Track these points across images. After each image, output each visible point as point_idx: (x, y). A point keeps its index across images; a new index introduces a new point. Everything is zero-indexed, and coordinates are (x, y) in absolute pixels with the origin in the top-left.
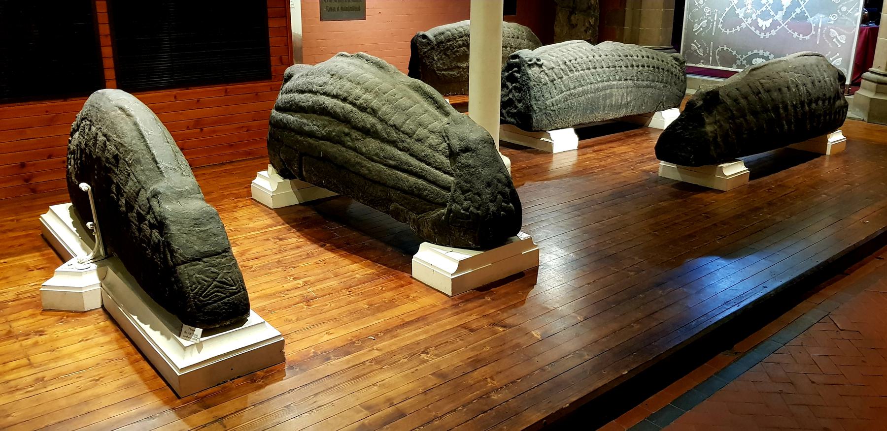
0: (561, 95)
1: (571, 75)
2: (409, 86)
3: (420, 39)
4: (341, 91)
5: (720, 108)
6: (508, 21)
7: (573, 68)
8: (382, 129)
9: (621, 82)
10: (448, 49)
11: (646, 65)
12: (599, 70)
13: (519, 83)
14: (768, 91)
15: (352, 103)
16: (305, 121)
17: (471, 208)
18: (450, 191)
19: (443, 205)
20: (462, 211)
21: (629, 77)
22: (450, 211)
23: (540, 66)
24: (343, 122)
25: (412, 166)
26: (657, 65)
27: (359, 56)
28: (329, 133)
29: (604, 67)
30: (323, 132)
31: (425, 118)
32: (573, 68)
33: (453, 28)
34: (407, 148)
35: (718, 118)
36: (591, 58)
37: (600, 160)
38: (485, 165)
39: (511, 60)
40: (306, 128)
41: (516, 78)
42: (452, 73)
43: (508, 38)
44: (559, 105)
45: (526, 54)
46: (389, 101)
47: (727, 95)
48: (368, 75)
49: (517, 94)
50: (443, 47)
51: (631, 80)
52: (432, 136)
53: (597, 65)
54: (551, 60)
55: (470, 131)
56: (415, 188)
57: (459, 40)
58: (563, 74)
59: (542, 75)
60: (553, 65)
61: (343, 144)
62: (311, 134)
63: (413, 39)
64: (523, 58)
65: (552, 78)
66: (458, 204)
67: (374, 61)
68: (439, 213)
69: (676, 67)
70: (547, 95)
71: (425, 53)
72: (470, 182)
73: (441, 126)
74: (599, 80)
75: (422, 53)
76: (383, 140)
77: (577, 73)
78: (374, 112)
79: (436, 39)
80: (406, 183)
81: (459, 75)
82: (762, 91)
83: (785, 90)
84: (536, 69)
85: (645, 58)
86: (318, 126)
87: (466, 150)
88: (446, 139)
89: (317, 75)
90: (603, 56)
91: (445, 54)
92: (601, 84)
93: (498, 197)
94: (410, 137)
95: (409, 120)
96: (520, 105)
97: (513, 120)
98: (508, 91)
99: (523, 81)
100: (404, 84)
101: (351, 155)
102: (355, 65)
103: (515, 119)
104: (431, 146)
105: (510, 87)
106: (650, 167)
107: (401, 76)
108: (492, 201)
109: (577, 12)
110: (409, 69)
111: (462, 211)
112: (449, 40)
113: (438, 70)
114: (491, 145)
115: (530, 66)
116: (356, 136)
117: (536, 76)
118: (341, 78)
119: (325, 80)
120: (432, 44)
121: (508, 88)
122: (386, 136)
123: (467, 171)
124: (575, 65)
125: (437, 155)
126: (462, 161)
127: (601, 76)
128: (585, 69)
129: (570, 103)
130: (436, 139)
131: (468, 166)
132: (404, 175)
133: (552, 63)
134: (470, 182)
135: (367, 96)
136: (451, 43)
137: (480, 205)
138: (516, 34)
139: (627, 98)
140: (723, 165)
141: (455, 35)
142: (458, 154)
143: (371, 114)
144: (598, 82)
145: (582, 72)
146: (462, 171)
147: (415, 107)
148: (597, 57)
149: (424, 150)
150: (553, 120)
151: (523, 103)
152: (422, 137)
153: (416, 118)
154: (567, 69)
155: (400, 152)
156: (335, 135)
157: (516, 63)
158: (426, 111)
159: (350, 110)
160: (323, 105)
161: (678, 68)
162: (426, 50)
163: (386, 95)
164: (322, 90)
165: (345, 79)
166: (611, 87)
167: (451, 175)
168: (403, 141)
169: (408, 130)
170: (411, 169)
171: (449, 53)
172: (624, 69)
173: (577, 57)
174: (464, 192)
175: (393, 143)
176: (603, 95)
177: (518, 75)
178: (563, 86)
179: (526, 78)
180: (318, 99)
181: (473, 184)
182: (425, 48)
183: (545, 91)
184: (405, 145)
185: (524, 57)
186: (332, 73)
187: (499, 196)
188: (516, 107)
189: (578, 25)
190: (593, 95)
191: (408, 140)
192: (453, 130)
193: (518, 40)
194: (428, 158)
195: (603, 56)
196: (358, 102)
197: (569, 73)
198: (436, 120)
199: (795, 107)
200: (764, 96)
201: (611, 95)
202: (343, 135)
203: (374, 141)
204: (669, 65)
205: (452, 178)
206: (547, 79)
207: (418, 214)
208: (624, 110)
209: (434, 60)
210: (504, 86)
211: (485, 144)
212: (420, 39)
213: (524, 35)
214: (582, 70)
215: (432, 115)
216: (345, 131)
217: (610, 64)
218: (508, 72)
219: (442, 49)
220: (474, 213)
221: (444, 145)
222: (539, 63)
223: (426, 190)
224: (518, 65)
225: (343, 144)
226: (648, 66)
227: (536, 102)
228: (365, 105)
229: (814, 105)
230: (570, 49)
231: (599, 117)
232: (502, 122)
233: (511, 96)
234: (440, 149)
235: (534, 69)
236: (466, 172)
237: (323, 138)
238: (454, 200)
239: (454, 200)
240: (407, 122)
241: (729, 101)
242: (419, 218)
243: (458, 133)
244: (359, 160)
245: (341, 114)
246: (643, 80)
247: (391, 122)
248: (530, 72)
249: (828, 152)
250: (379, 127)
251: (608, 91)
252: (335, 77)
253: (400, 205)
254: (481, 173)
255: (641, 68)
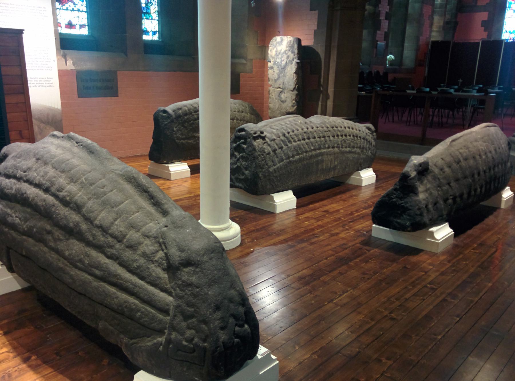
0: (281, 163)
1: (290, 145)
2: (121, 176)
3: (161, 113)
4: (44, 179)
5: (429, 177)
6: (234, 99)
7: (291, 139)
8: (87, 230)
9: (329, 150)
10: (185, 121)
11: (348, 134)
12: (312, 140)
13: (246, 153)
14: (466, 159)
15: (54, 195)
16: (9, 211)
17: (196, 340)
18: (168, 315)
19: (160, 332)
20: (184, 343)
21: (336, 145)
22: (169, 341)
23: (264, 138)
24: (45, 217)
25: (122, 279)
26: (356, 134)
27: (70, 138)
28: (31, 228)
29: (316, 137)
30: (24, 226)
31: (137, 217)
32: (291, 139)
33: (189, 104)
34: (115, 255)
35: (429, 186)
36: (305, 130)
37: (318, 219)
38: (213, 282)
39: (238, 133)
40: (9, 219)
41: (243, 149)
42: (190, 141)
43: (235, 113)
44: (280, 172)
45: (251, 127)
46: (97, 196)
47: (435, 165)
48: (75, 161)
49: (244, 163)
50: (181, 120)
51: (337, 147)
52: (147, 241)
53: (311, 136)
54: (273, 133)
55: (194, 238)
56: (125, 307)
57: (194, 114)
58: (283, 145)
59: (265, 146)
60: (274, 137)
61: (44, 242)
62: (13, 227)
63: (155, 114)
64: (248, 131)
65: (274, 148)
66: (178, 333)
67: (84, 144)
68: (155, 341)
69: (369, 135)
70: (270, 163)
71: (166, 125)
72: (192, 305)
73: (157, 230)
74: (312, 148)
75: (163, 125)
76: (88, 244)
77: (294, 144)
78: (78, 208)
79: (175, 113)
80: (115, 300)
81: (195, 143)
82: (462, 159)
83: (478, 157)
84: (260, 141)
85: (347, 129)
86: (20, 219)
87: (187, 263)
88: (164, 247)
89: (23, 158)
90: (315, 128)
91: (183, 126)
92: (314, 153)
93: (230, 321)
94: (119, 242)
95: (118, 220)
96: (247, 172)
97: (241, 185)
98: (236, 160)
99: (250, 151)
100: (116, 173)
101: (52, 257)
102: (63, 148)
103: (243, 184)
104: (144, 255)
105: (238, 157)
106: (361, 225)
107: (113, 163)
108: (222, 328)
109: (286, 92)
110: (153, 138)
111: (184, 343)
112: (186, 114)
113: (177, 139)
114: (220, 255)
115: (255, 138)
116: (58, 236)
117: (260, 146)
118: (46, 163)
119: (30, 165)
120: (172, 118)
121: (236, 157)
122: (91, 239)
123: (189, 290)
124: (293, 136)
125: (152, 266)
126: (183, 278)
127: (314, 145)
128: (301, 139)
129: (289, 170)
130: (151, 246)
131: (191, 285)
132: (112, 290)
133: (273, 135)
134: (192, 305)
135: (72, 188)
136: (188, 116)
137: (207, 336)
138: (241, 109)
139: (334, 163)
140: (432, 229)
141: (191, 110)
142: (178, 269)
143: (75, 210)
144: (312, 150)
145: (298, 142)
146: (184, 291)
147: (127, 204)
148: (310, 129)
149: (136, 260)
150: (275, 184)
151: (249, 171)
152: (134, 243)
153: (127, 218)
154: (286, 140)
155: (107, 261)
156: (37, 232)
157: (243, 135)
158: (140, 208)
159: (52, 203)
160: (25, 195)
161: (371, 135)
162: (166, 123)
163: (94, 186)
164: (26, 176)
165: (50, 166)
166: (322, 154)
167: (170, 294)
168: (111, 247)
169: (117, 233)
170: (120, 283)
171: (186, 125)
172: (332, 138)
173: (294, 129)
174: (186, 317)
175: (100, 248)
176: (316, 161)
177: (245, 146)
178: (283, 155)
179: (251, 149)
180: (21, 186)
181: (198, 308)
182: (166, 121)
183: (268, 160)
184: (114, 251)
185: (249, 130)
186: (38, 157)
187: (231, 320)
188: (243, 174)
189: (287, 101)
190: (307, 161)
191: (118, 246)
192: (172, 235)
193: (243, 114)
194: (141, 271)
195: (315, 128)
196: (61, 194)
197: (288, 144)
198: (152, 220)
199: (485, 172)
200: (463, 163)
201: (322, 161)
202: (45, 232)
203: (78, 243)
204: (365, 134)
205: (171, 299)
206: (270, 149)
207: (132, 339)
208: (332, 172)
209: (174, 131)
210: (232, 155)
211: (212, 254)
212: (161, 113)
213: (247, 110)
214: (298, 141)
215: (149, 215)
216: (46, 228)
217: (321, 135)
218: (236, 143)
219: (181, 121)
220: (199, 346)
221: (161, 254)
222: (262, 135)
223: (139, 311)
224: (244, 138)
225: (44, 242)
226: (350, 136)
227: (261, 170)
228: (68, 198)
229: (496, 169)
230: (288, 122)
231: (312, 179)
232: (232, 186)
233: (239, 164)
234: (156, 259)
235: (258, 141)
236: (189, 293)
237: (24, 233)
238: (173, 328)
239: (173, 328)
240: (116, 223)
241: (436, 171)
242: (132, 344)
243: (177, 240)
244: (61, 265)
245: (42, 208)
246: (346, 147)
247: (97, 222)
248: (255, 143)
249: (503, 206)
250: (84, 226)
251: (320, 158)
252: (40, 162)
253: (110, 325)
254: (207, 294)
255: (344, 137)
